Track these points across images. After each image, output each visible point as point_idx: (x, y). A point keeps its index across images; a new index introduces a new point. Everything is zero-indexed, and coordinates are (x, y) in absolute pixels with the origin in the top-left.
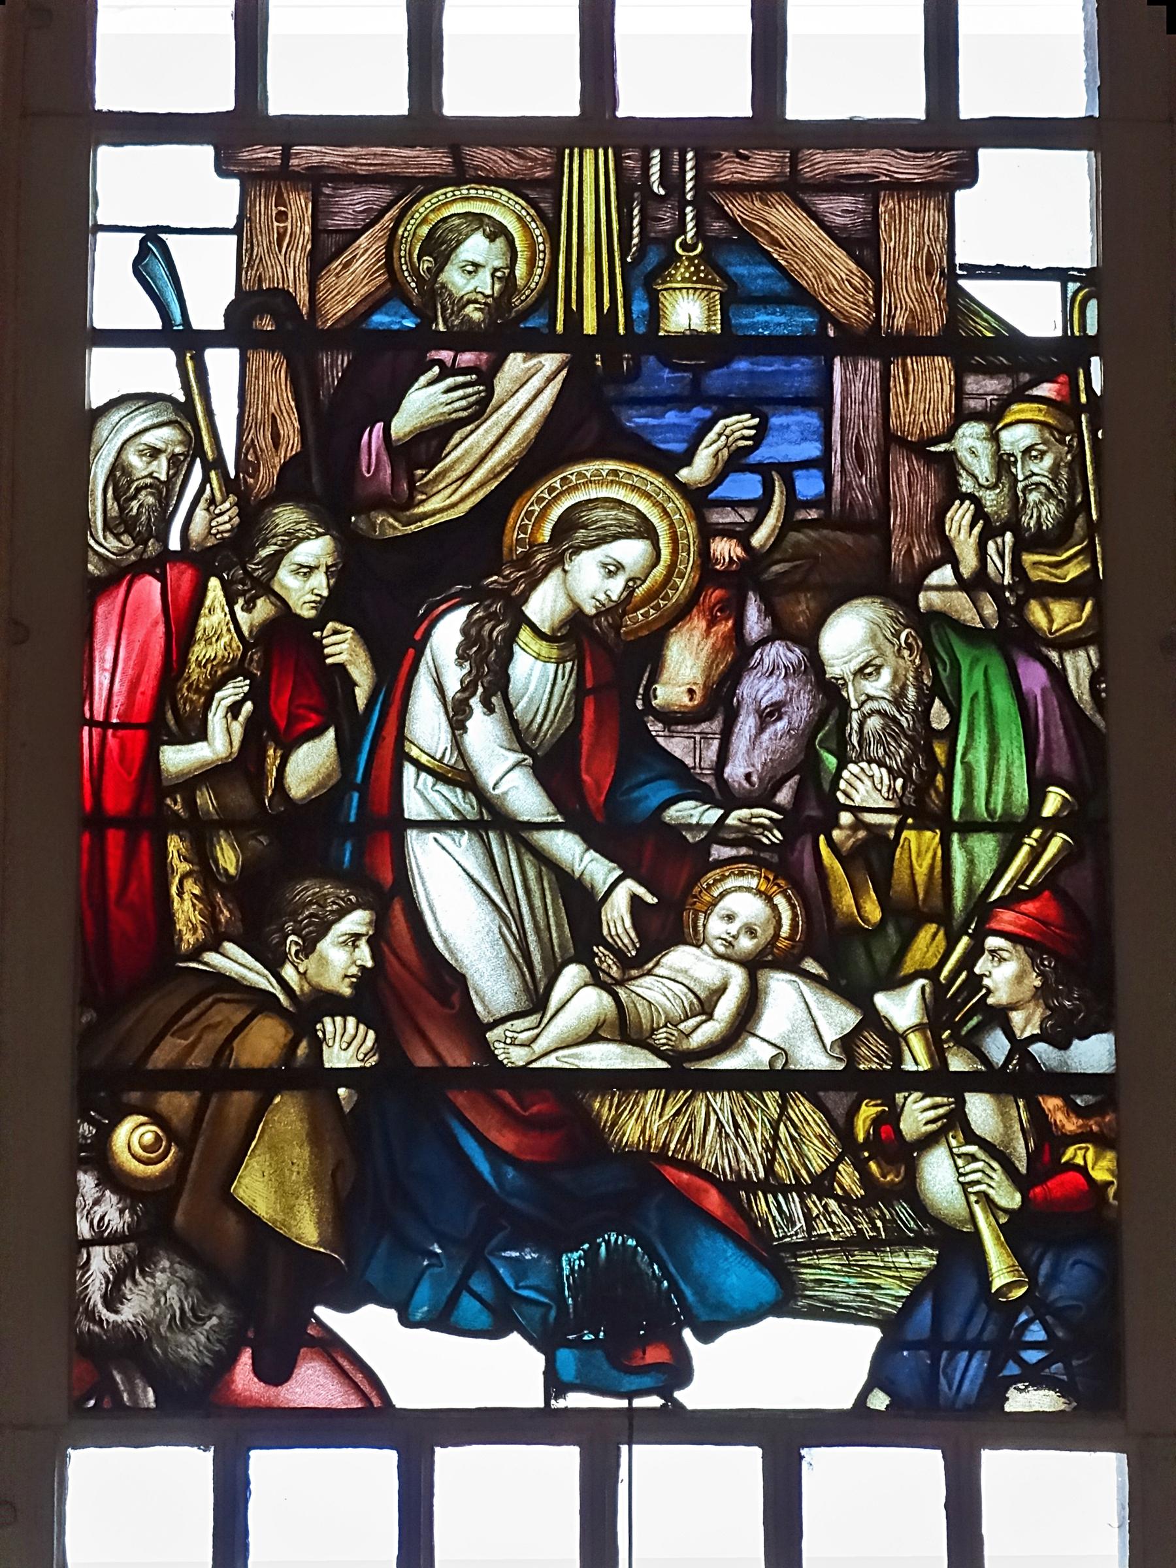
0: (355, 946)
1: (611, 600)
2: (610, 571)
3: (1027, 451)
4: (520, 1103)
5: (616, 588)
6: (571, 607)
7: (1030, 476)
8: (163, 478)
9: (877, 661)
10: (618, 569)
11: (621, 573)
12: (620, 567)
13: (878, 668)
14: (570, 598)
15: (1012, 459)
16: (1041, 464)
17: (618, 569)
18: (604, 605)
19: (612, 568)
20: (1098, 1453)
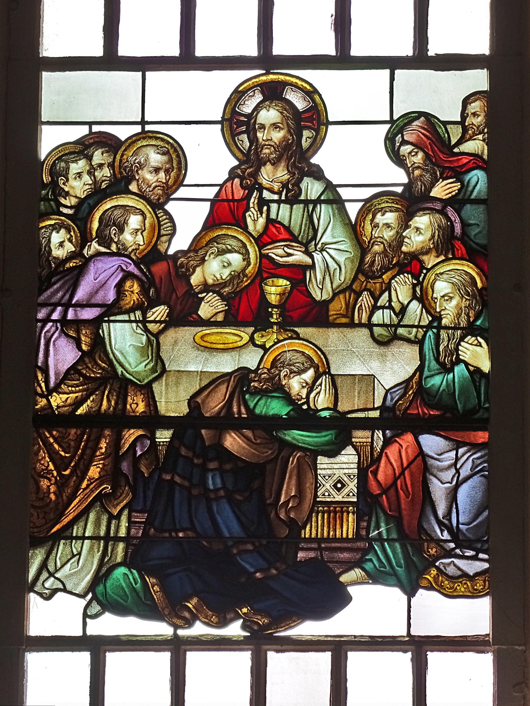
0: (136, 235)
1: (222, 279)
2: (224, 266)
3: (410, 153)
4: (145, 598)
5: (226, 273)
6: (202, 280)
7: (413, 164)
8: (164, 181)
9: (451, 295)
10: (229, 265)
11: (230, 267)
12: (229, 264)
13: (451, 298)
14: (205, 278)
15: (404, 158)
16: (417, 158)
17: (229, 265)
18: (218, 280)
19: (226, 264)
20: (67, 73)
